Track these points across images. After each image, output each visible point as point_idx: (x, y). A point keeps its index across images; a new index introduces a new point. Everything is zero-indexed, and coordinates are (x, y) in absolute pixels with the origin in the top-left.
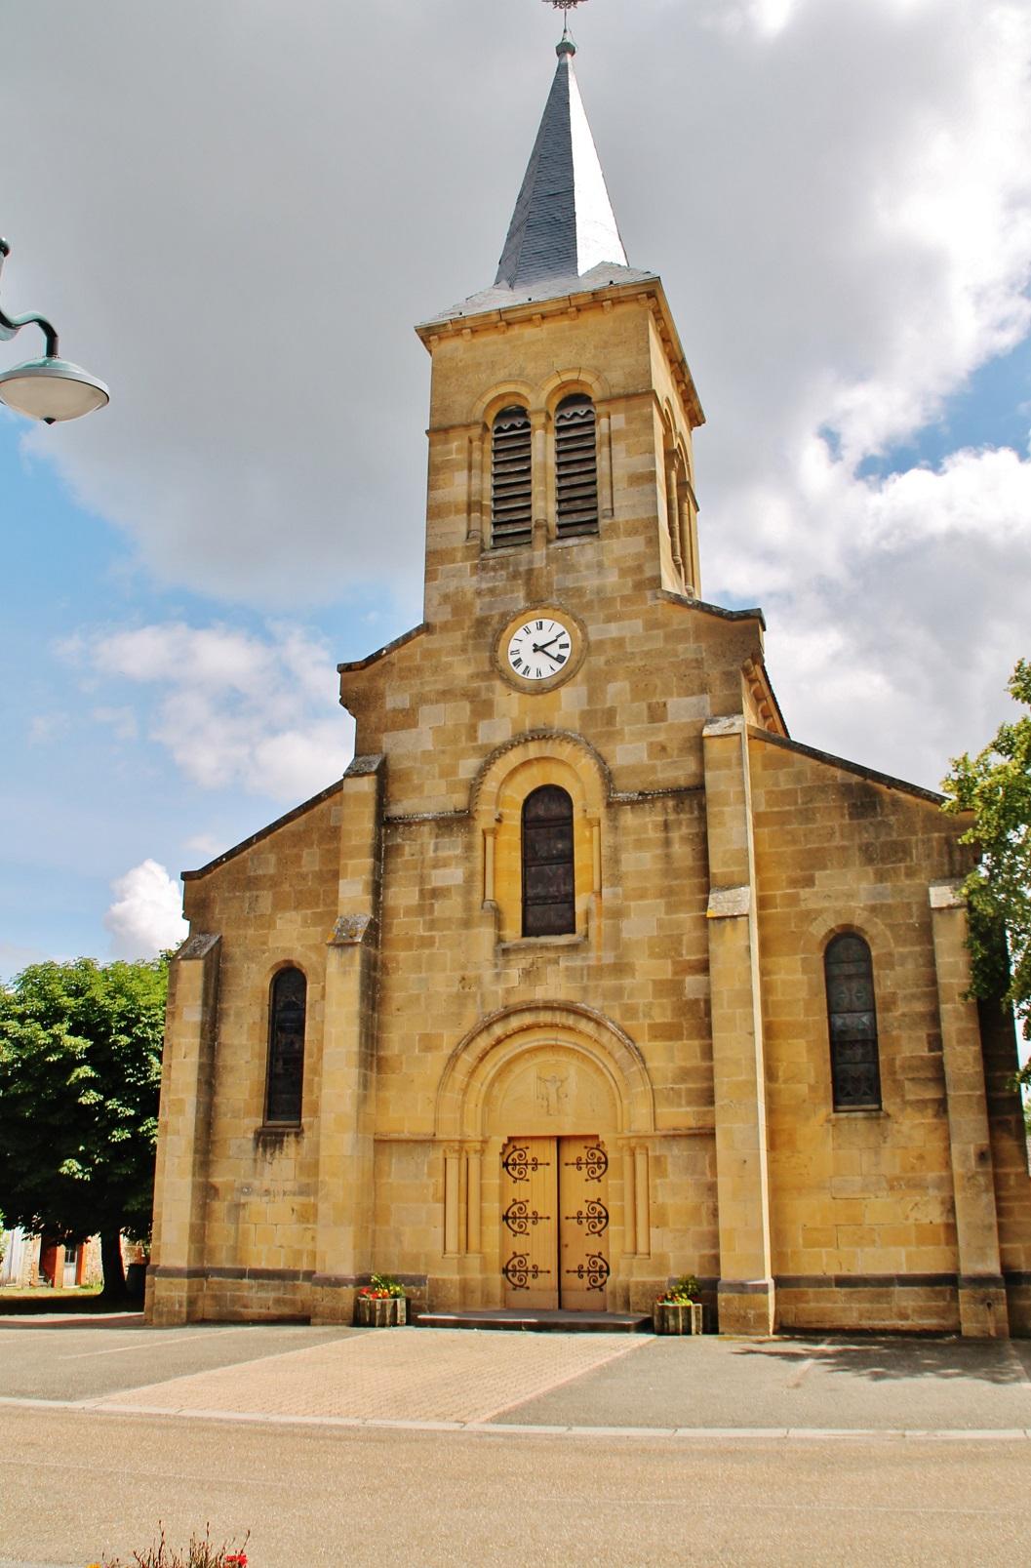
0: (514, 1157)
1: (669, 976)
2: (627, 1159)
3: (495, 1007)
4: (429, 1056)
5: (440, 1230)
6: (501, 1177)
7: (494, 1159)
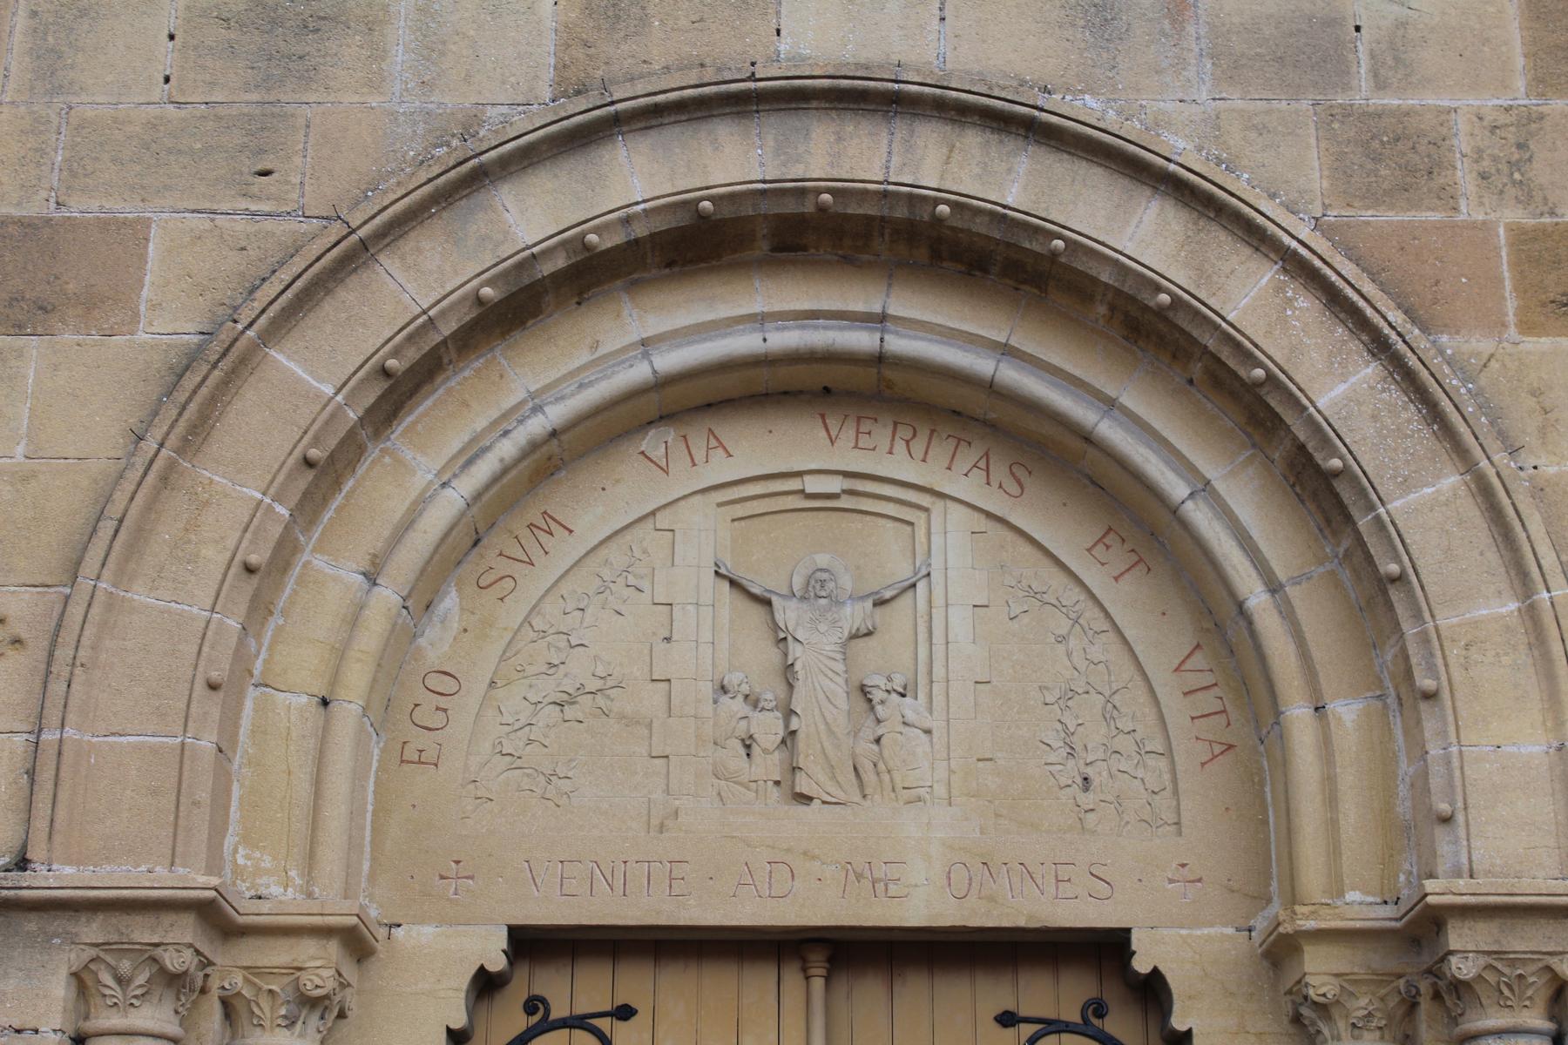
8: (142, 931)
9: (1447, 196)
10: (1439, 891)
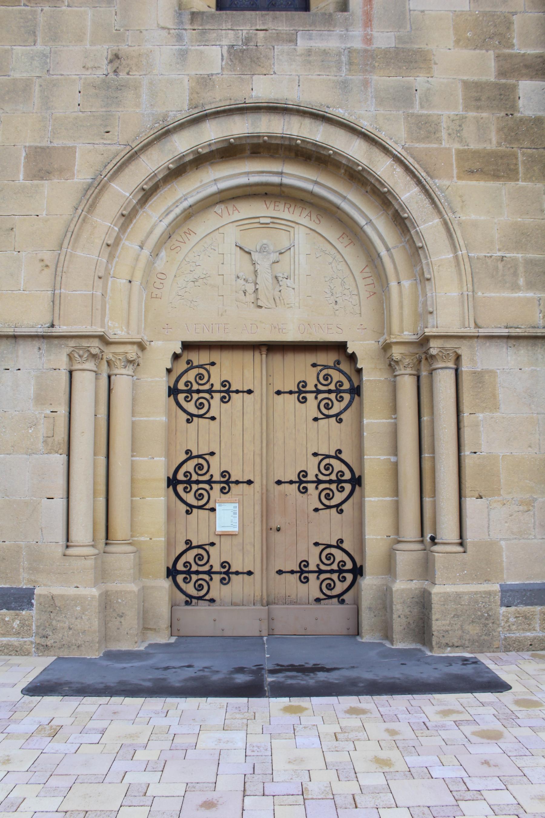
0: (196, 374)
1: (492, 78)
2: (407, 384)
3: (178, 107)
4: (46, 186)
5: (59, 504)
6: (169, 414)
7: (155, 379)
8: (85, 343)
9: (439, 140)
10: (429, 331)
